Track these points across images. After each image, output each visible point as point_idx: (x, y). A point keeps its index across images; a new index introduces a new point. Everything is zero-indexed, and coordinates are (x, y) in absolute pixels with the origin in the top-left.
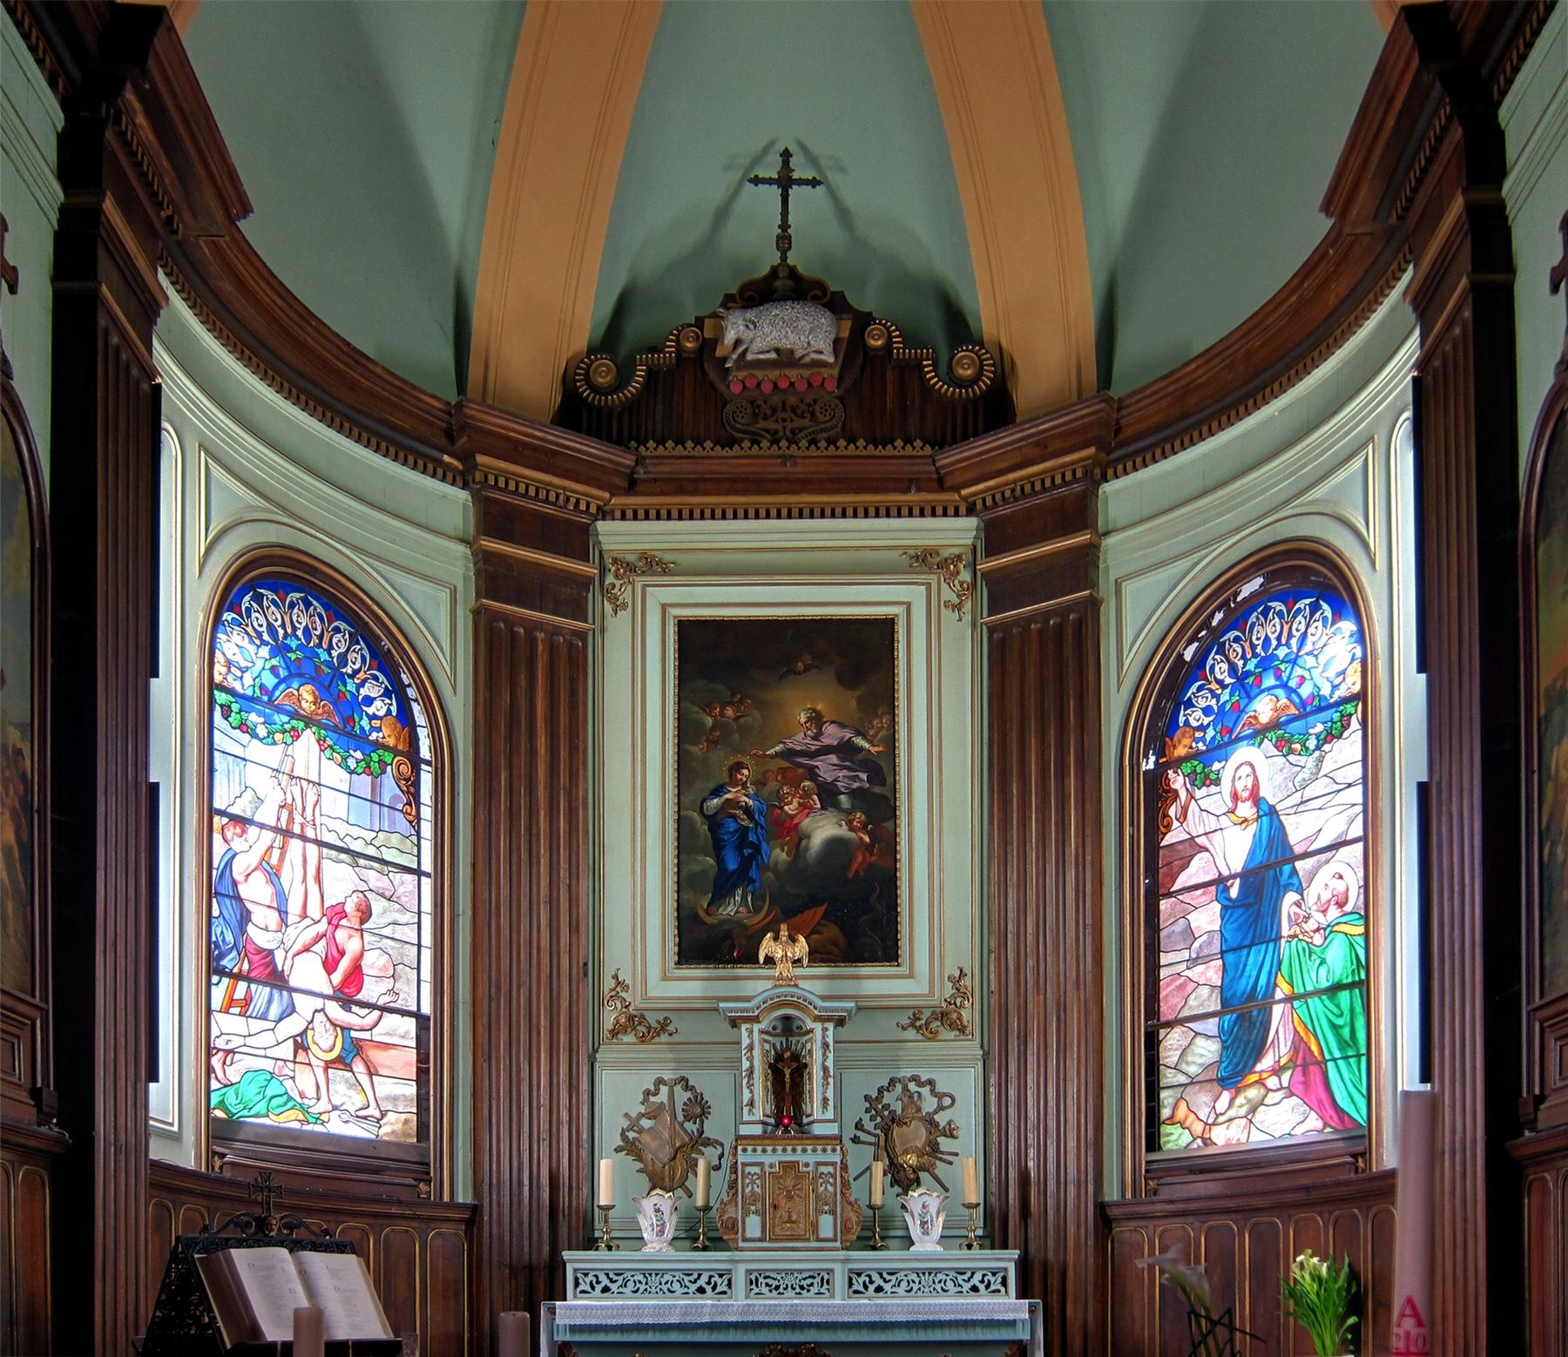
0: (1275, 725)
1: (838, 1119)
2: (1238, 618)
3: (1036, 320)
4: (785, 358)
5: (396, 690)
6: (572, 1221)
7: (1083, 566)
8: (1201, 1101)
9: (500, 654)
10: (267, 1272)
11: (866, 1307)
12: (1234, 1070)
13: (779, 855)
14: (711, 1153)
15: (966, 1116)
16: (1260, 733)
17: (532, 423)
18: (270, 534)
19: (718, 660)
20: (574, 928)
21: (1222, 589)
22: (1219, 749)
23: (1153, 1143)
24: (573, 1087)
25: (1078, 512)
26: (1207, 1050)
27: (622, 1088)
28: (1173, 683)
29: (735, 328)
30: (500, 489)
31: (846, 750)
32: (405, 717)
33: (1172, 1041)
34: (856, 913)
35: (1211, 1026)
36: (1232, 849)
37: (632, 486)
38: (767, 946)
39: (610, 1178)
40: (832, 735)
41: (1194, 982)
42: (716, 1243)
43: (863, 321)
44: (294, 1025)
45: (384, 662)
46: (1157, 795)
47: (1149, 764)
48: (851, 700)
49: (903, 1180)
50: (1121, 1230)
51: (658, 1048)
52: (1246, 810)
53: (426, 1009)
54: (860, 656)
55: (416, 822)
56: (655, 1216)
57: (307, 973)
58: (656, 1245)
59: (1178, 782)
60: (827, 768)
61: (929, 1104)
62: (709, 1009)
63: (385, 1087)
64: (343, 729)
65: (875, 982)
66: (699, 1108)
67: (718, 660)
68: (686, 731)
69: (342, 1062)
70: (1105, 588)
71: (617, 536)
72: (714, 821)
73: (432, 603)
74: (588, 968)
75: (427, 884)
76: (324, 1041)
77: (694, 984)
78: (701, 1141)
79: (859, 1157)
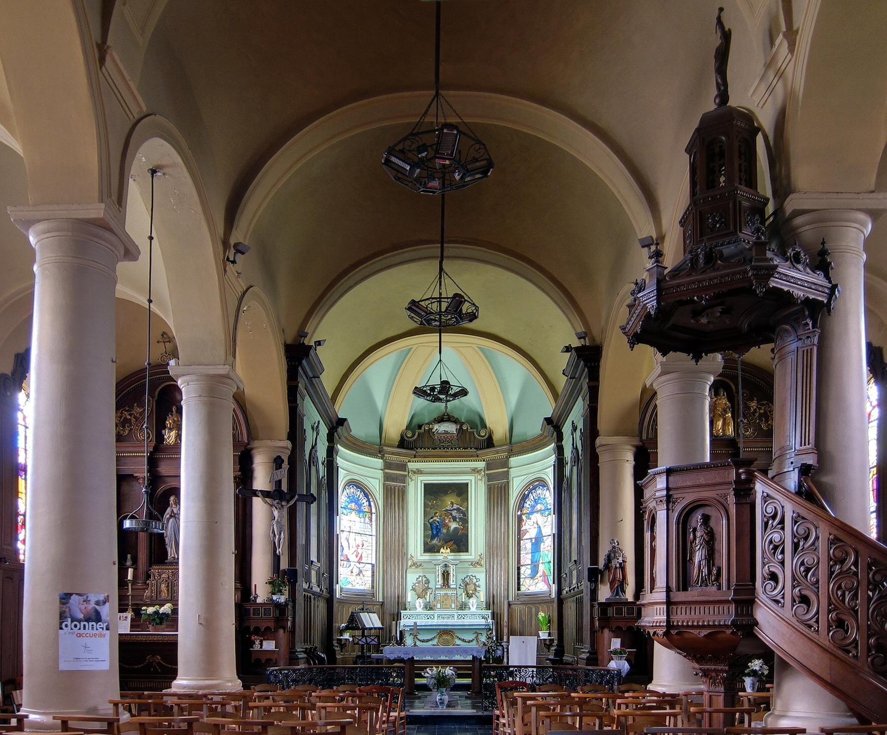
0: (541, 510)
1: (456, 584)
2: (534, 488)
3: (497, 423)
4: (446, 432)
5: (368, 500)
6: (402, 604)
7: (507, 474)
8: (528, 581)
9: (388, 492)
10: (365, 617)
11: (461, 622)
12: (533, 576)
13: (445, 531)
14: (430, 591)
15: (482, 583)
16: (537, 512)
17: (394, 447)
18: (349, 478)
19: (433, 491)
20: (403, 546)
21: (527, 487)
22: (532, 513)
23: (519, 589)
24: (402, 578)
25: (505, 464)
26: (529, 572)
27: (412, 578)
28: (524, 498)
29: (436, 427)
30: (474, 672)
31: (458, 510)
32: (370, 505)
33: (523, 569)
34: (460, 543)
35: (529, 567)
36: (532, 533)
37: (415, 457)
38: (442, 550)
39: (410, 596)
40: (455, 506)
41: (526, 559)
42: (431, 609)
43: (462, 424)
44: (350, 568)
45: (366, 495)
46: (520, 520)
47: (519, 513)
48: (459, 499)
49: (469, 596)
50: (513, 606)
51: (419, 569)
52: (536, 525)
53: (374, 562)
54: (461, 490)
55: (371, 525)
56: (419, 603)
57: (353, 558)
58: (419, 610)
59: (524, 517)
60: (454, 513)
61: (475, 581)
62: (430, 562)
63: (366, 578)
64: (359, 511)
65: (463, 556)
66: (428, 582)
67: (433, 491)
68: (426, 506)
69: (359, 574)
70: (511, 478)
71: (412, 466)
72: (431, 524)
73: (376, 485)
74: (406, 554)
75: (374, 538)
76: (356, 571)
77: (427, 557)
78: (428, 588)
79: (460, 591)
